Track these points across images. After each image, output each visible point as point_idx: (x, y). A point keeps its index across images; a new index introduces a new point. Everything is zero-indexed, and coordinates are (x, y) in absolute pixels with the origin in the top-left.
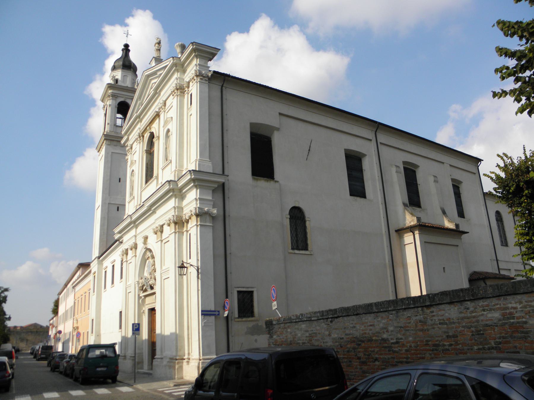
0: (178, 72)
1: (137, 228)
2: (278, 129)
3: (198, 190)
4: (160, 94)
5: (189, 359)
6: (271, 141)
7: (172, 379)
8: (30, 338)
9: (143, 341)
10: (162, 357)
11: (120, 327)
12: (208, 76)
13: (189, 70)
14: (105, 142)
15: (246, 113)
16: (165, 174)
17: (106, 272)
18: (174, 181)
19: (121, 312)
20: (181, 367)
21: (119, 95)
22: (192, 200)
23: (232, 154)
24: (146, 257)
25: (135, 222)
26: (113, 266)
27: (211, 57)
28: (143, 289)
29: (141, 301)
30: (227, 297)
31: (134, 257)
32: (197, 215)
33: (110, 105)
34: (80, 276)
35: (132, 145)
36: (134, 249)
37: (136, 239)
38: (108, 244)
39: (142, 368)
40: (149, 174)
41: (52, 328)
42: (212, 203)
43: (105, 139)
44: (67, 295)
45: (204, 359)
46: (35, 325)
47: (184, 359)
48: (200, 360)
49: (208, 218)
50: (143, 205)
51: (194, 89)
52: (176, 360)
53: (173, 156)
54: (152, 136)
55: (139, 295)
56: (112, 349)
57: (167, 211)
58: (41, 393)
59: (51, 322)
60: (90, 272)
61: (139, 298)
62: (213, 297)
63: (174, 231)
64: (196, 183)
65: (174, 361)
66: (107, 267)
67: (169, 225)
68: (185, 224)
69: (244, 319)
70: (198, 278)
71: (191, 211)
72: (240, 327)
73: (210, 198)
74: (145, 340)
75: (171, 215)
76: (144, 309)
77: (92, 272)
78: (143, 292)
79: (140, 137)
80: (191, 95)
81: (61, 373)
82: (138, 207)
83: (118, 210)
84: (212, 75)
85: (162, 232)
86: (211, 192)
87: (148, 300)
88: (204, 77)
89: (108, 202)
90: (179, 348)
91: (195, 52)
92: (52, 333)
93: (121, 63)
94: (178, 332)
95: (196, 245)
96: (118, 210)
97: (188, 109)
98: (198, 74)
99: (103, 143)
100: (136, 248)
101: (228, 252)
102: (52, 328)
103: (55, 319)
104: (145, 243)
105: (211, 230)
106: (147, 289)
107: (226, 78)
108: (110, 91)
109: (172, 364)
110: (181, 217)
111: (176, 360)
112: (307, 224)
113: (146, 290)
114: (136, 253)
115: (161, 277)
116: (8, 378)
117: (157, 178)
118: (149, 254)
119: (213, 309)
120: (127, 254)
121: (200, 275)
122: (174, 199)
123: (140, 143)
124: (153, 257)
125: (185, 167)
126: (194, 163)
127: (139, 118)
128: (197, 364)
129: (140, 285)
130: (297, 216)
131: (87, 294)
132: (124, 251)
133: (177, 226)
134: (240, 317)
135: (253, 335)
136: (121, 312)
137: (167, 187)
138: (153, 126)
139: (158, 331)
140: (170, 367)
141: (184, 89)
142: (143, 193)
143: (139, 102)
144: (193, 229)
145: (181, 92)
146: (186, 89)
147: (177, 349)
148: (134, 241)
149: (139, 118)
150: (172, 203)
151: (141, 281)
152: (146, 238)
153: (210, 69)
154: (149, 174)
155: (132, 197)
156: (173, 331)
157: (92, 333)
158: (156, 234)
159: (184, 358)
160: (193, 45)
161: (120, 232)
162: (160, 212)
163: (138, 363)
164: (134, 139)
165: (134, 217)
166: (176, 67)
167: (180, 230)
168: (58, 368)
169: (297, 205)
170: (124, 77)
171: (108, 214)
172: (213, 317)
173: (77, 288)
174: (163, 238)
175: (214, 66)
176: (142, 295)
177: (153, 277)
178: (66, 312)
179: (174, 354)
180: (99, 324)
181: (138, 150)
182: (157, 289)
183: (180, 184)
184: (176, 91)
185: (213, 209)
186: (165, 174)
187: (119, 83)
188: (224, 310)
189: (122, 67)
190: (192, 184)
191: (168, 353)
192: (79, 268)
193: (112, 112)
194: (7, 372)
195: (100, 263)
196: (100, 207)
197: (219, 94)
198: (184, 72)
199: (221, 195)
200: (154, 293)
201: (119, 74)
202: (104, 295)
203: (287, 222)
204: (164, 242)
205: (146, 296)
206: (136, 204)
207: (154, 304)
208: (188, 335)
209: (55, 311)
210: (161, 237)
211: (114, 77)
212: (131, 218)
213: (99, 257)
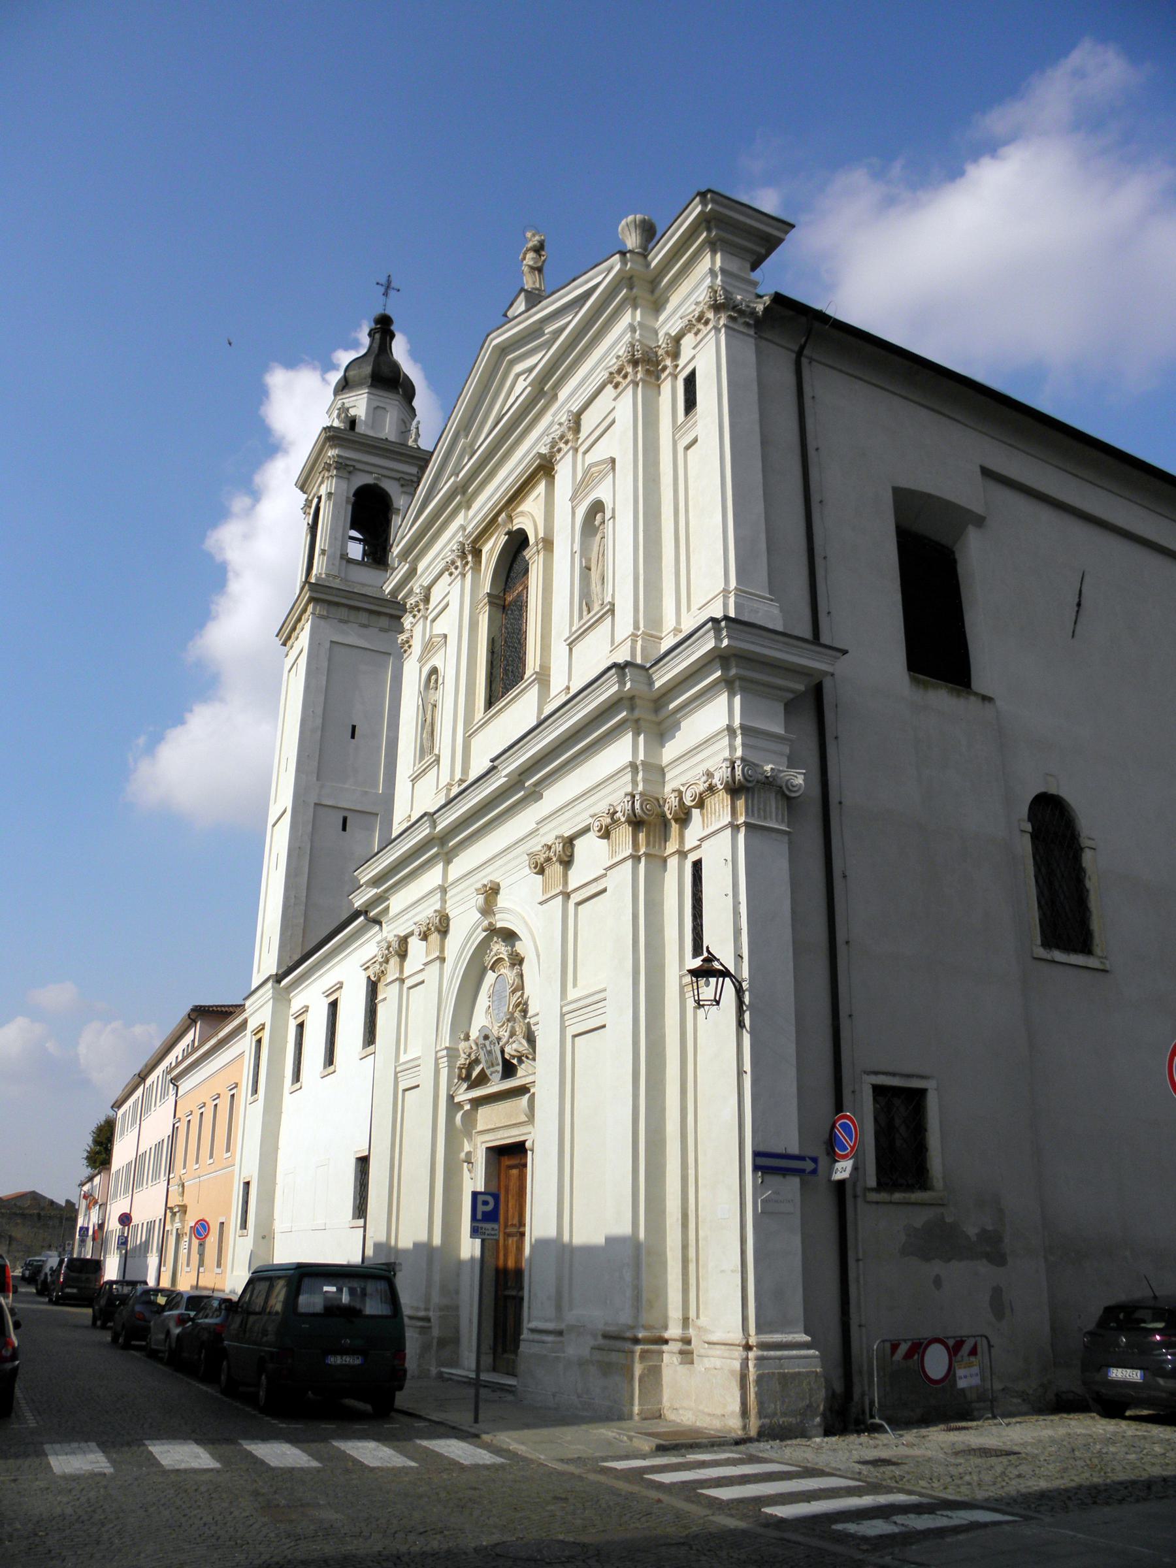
0: (635, 308)
1: (448, 862)
2: (979, 521)
3: (737, 700)
4: (555, 397)
5: (687, 1341)
6: (955, 561)
7: (621, 1418)
8: (20, 1232)
9: (460, 1263)
10: (562, 1326)
11: (361, 1209)
12: (753, 313)
13: (674, 300)
14: (310, 608)
15: (881, 452)
16: (572, 658)
17: (301, 1026)
18: (641, 667)
19: (363, 1163)
20: (654, 1373)
21: (359, 466)
22: (709, 735)
23: (839, 583)
24: (489, 960)
25: (442, 839)
26: (334, 1005)
27: (763, 251)
28: (471, 1076)
29: (458, 1121)
30: (839, 1107)
31: (438, 963)
32: (734, 790)
33: (330, 494)
34: (195, 1050)
35: (429, 588)
36: (434, 937)
37: (443, 901)
38: (315, 932)
39: (455, 1362)
40: (505, 668)
41: (88, 1208)
42: (787, 750)
43: (311, 600)
44: (144, 1109)
45: (763, 1346)
46: (34, 1196)
47: (666, 1342)
48: (748, 1347)
49: (773, 803)
50: (493, 768)
51: (707, 356)
52: (636, 1341)
53: (622, 588)
54: (518, 542)
55: (451, 1098)
56: (382, 1286)
57: (606, 774)
58: (140, 1443)
59: (86, 1188)
60: (243, 1025)
61: (453, 1106)
62: (795, 1102)
63: (629, 851)
64: (733, 672)
65: (628, 1346)
66: (306, 1009)
67: (606, 834)
68: (675, 827)
69: (898, 1196)
70: (740, 1024)
71: (709, 775)
72: (882, 1224)
73: (779, 729)
74: (472, 1259)
75: (617, 796)
76: (467, 1147)
77: (252, 1025)
78: (469, 1088)
79: (463, 556)
80: (690, 381)
81: (153, 1354)
82: (455, 791)
83: (344, 829)
84: (766, 309)
85: (567, 862)
86: (780, 708)
87: (487, 1116)
88: (741, 313)
89: (313, 799)
90: (645, 1296)
91: (709, 230)
92: (88, 1219)
93: (367, 369)
94: (642, 1235)
95: (730, 900)
96: (344, 829)
97: (676, 428)
98: (721, 300)
99: (304, 611)
100: (444, 931)
101: (841, 937)
102: (88, 1208)
103: (97, 1180)
104: (488, 909)
105: (784, 848)
106: (491, 1072)
107: (817, 324)
108: (331, 453)
109: (614, 1357)
110: (659, 802)
111: (628, 1344)
112: (1087, 858)
113: (483, 1079)
114: (442, 950)
115: (563, 1029)
116: (9, 1366)
117: (543, 678)
118: (499, 948)
119: (794, 1150)
120: (403, 955)
121: (747, 1016)
122: (629, 737)
123: (464, 575)
124: (517, 961)
125: (669, 622)
126: (720, 600)
127: (464, 492)
128: (737, 1365)
129: (462, 1060)
130: (1053, 827)
131: (224, 1104)
132: (395, 945)
133: (642, 836)
134: (881, 1186)
135: (927, 1258)
136: (363, 1163)
137: (610, 689)
138: (522, 508)
139: (540, 1222)
140: (607, 1369)
141: (658, 363)
142: (475, 742)
144: (717, 844)
145: (648, 372)
146: (668, 362)
147: (637, 1298)
148: (438, 906)
149: (464, 493)
150: (621, 752)
151: (462, 1046)
152: (492, 892)
153: (760, 291)
154: (505, 668)
155: (429, 759)
156: (624, 1228)
157: (244, 1225)
158: (541, 871)
159: (667, 1335)
161: (376, 881)
162: (556, 795)
163: (442, 1343)
164: (442, 565)
166: (631, 288)
167: (652, 852)
168: (144, 1338)
169: (1053, 791)
170: (375, 411)
171: (312, 841)
172: (795, 1182)
173: (185, 1085)
174: (572, 886)
175: (779, 276)
176: (464, 1095)
177: (520, 1029)
178: (140, 1159)
179: (625, 1318)
180: (268, 1198)
181: (454, 600)
182: (541, 1073)
183: (662, 678)
184: (630, 369)
185: (792, 772)
186: (572, 658)
187: (361, 429)
188: (833, 1158)
189: (370, 381)
190: (719, 673)
191: (593, 1313)
192: (194, 1022)
193: (335, 517)
194: (7, 1343)
195: (282, 998)
196: (287, 817)
197: (790, 378)
198: (658, 306)
199: (810, 728)
200: (523, 1090)
201: (359, 403)
202: (290, 1102)
203: (1024, 846)
205: (477, 1103)
206: (445, 779)
207: (523, 1130)
208: (685, 1247)
209: (100, 1154)
210: (566, 883)
211: (344, 410)
212: (434, 825)
213: (278, 978)
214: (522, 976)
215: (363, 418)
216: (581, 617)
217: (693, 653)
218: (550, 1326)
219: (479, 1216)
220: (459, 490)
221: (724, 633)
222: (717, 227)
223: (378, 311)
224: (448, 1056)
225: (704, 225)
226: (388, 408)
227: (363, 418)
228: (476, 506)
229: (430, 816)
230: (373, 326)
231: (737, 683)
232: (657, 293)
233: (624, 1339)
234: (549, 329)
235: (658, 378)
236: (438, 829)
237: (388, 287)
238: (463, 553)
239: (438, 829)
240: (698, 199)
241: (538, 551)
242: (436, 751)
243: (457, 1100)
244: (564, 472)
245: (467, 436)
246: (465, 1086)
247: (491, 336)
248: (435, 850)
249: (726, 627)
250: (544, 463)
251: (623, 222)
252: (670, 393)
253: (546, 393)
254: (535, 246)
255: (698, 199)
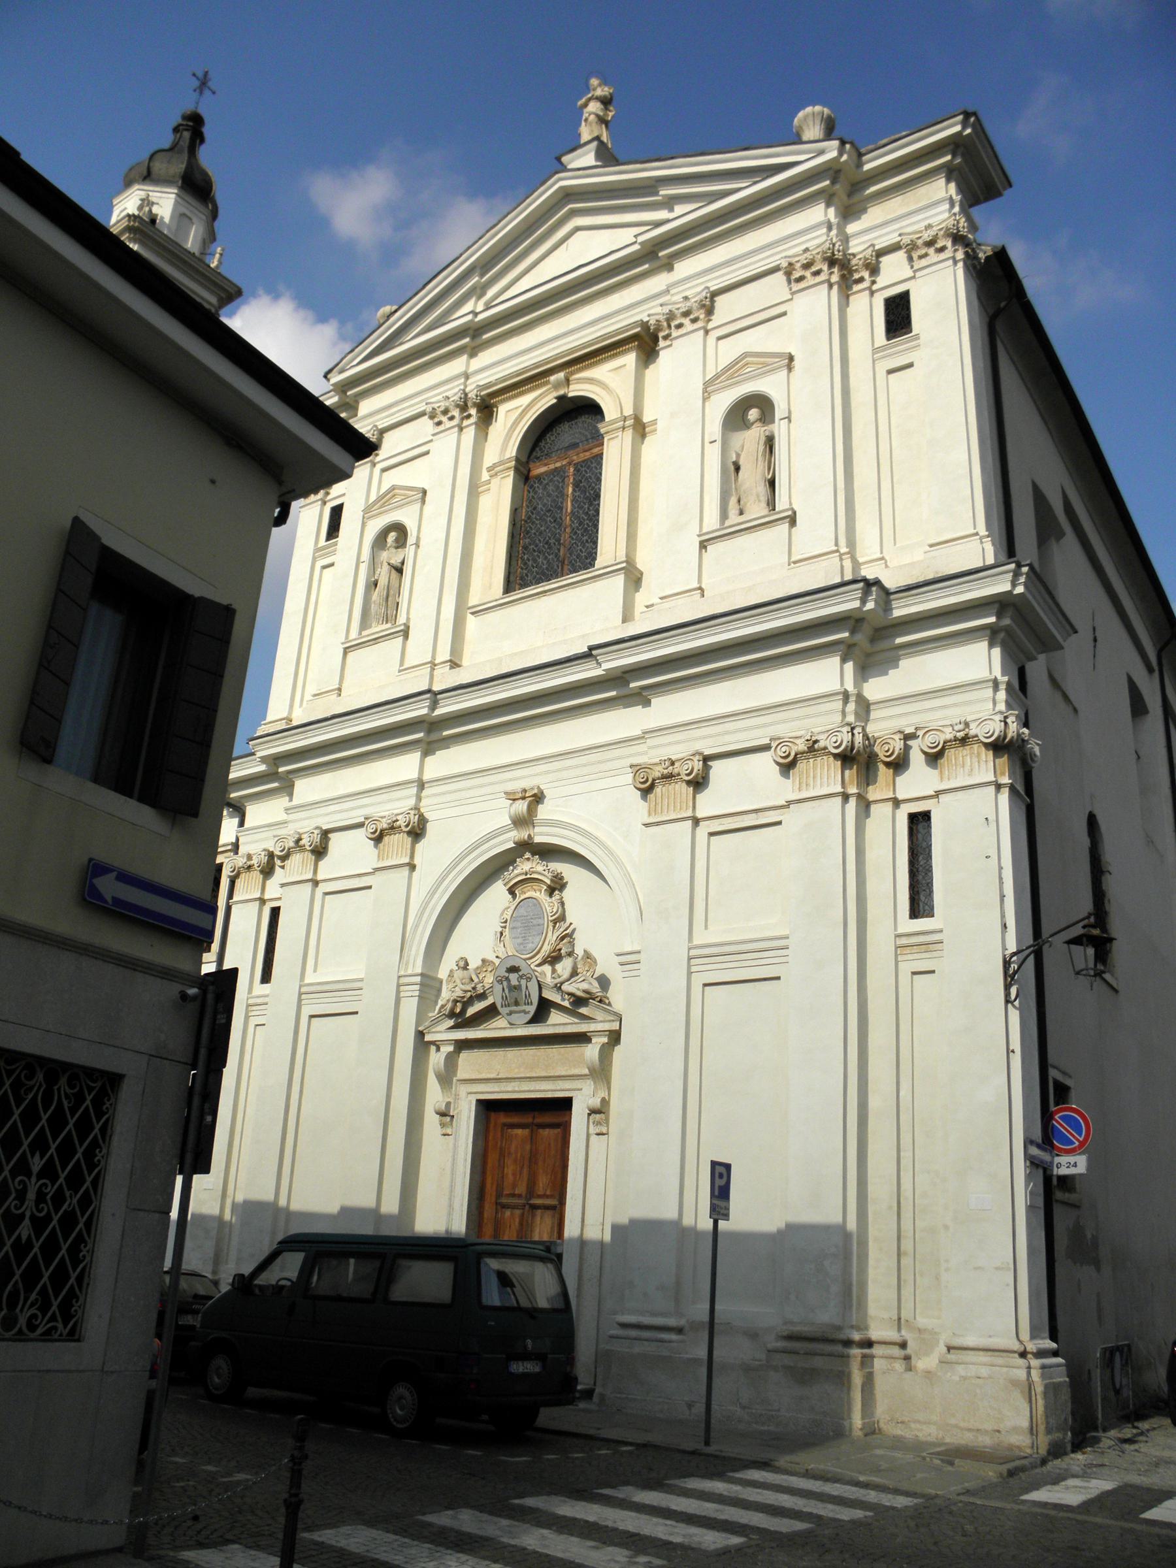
0: (828, 205)
1: (427, 753)
4: (669, 267)
10: (682, 1322)
64: (1007, 621)
84: (987, 258)
100: (417, 832)
104: (520, 822)
114: (412, 856)
115: (247, 1018)
137: (848, 603)
140: (805, 1377)
143: (475, 279)
160: (965, 124)
165: (446, 708)
166: (834, 182)
170: (180, 217)
198: (849, 212)
204: (322, 888)
205: (463, 1045)
210: (315, 871)
212: (434, 705)
214: (563, 904)
215: (167, 220)
216: (724, 515)
217: (970, 590)
218: (672, 1322)
219: (716, 1193)
220: (471, 332)
221: (1022, 579)
222: (963, 155)
223: (189, 108)
224: (422, 984)
225: (951, 147)
226: (195, 220)
227: (167, 220)
228: (486, 357)
229: (434, 696)
230: (180, 121)
231: (1002, 635)
232: (856, 198)
233: (832, 1341)
234: (665, 192)
235: (849, 288)
236: (437, 712)
237: (203, 83)
238: (466, 405)
239: (437, 712)
240: (960, 117)
241: (624, 428)
242: (402, 619)
243: (428, 1038)
244: (681, 359)
245: (482, 276)
246: (451, 1023)
247: (557, 176)
248: (422, 735)
249: (1027, 574)
250: (643, 334)
251: (809, 109)
252: (867, 312)
253: (658, 258)
254: (605, 97)
255: (960, 117)
